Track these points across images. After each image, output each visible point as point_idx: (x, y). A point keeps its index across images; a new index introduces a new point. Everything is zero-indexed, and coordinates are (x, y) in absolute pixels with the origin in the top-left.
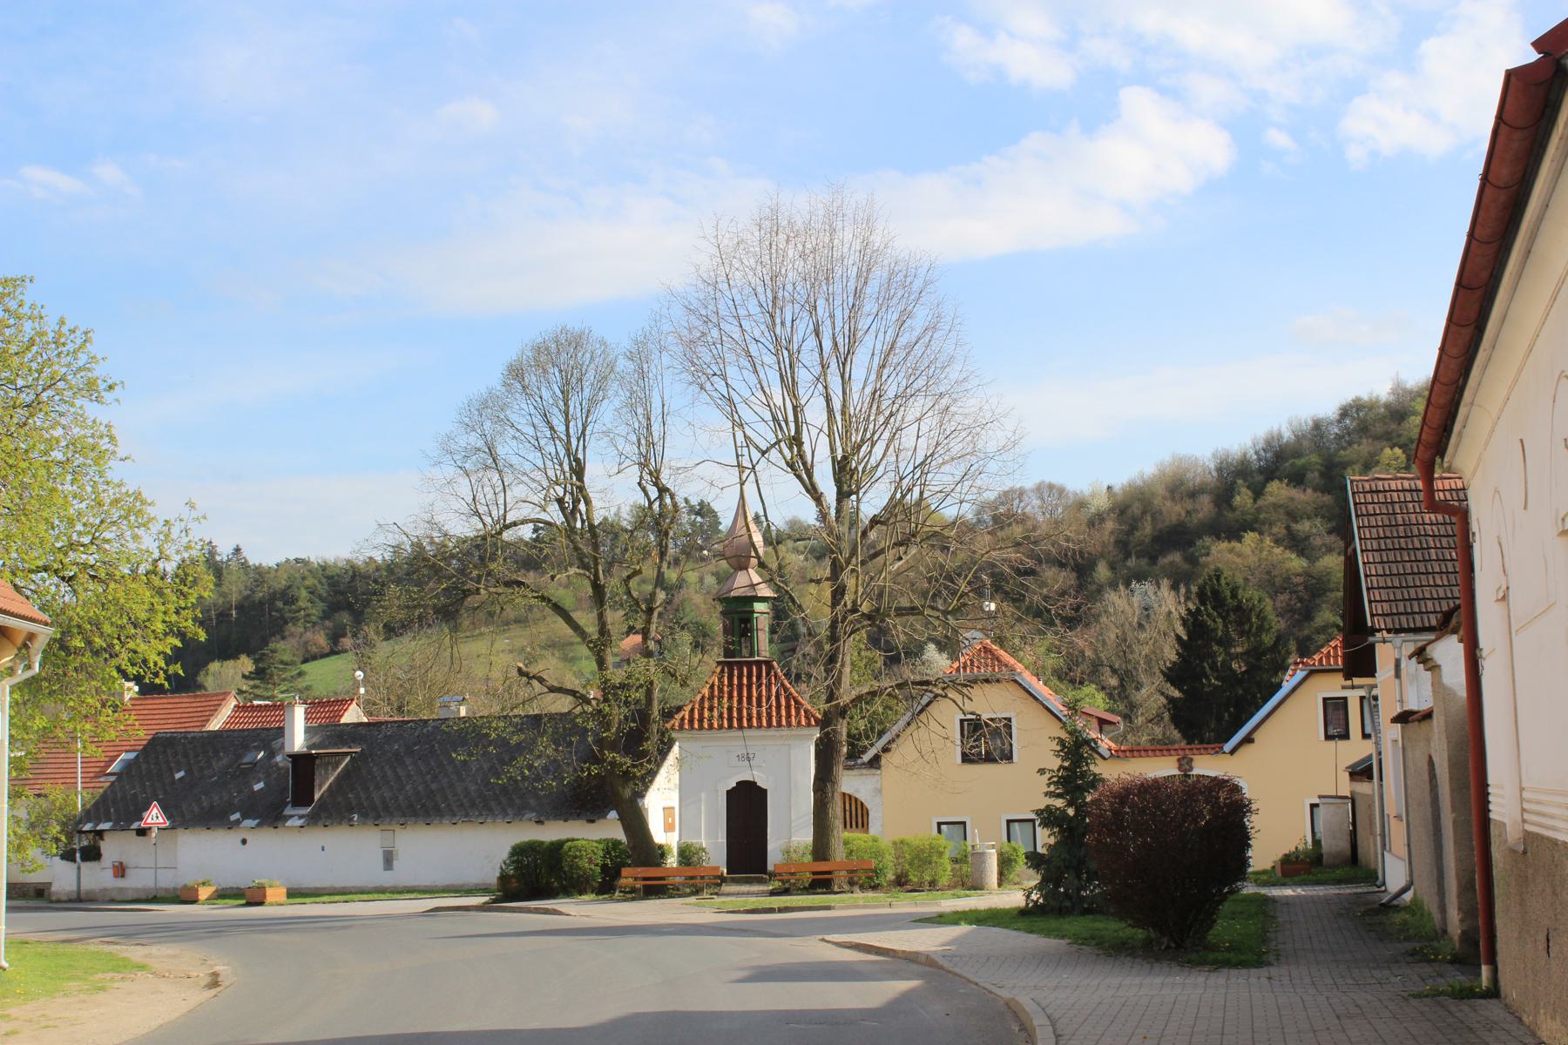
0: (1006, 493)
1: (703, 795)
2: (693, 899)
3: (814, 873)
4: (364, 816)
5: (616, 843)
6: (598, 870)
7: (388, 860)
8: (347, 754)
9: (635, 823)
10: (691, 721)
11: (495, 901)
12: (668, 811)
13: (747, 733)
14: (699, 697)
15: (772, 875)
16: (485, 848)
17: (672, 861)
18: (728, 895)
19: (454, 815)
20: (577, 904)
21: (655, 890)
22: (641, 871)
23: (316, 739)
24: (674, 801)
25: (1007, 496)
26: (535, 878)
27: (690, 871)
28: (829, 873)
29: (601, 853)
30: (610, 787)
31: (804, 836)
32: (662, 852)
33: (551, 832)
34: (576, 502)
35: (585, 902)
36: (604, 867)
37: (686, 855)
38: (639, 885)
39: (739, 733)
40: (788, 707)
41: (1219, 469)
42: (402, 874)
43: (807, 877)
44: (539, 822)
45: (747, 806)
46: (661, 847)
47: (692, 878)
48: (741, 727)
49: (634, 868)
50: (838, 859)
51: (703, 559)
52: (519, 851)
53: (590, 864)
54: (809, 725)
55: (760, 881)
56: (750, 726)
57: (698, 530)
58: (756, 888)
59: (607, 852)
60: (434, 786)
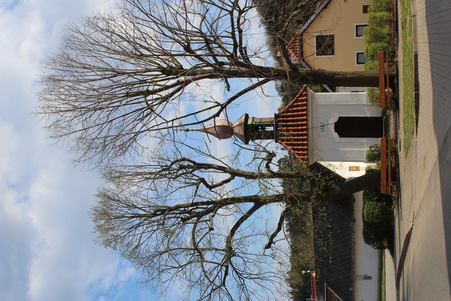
0: (276, 89)
1: (341, 149)
2: (401, 154)
3: (386, 86)
4: (350, 286)
5: (365, 195)
6: (379, 204)
7: (368, 278)
8: (327, 288)
9: (356, 183)
10: (303, 155)
11: (393, 253)
12: (351, 169)
13: (310, 126)
14: (292, 151)
15: (384, 113)
16: (365, 255)
17: (373, 165)
18: (396, 134)
19: (351, 253)
20: (400, 219)
21: (394, 175)
22: (383, 182)
23: (322, 298)
24: (347, 165)
25: (277, 89)
26: (382, 233)
27: (383, 155)
28: (385, 76)
29: (371, 202)
30: (339, 193)
31: (363, 95)
32: (369, 171)
33: (359, 226)
34: (184, 212)
35: (399, 214)
36: (378, 201)
37: (371, 158)
38: (390, 184)
39: (310, 130)
40: (298, 106)
41: (269, 35)
42: (373, 272)
43: (388, 90)
44: (354, 221)
45: (349, 127)
46: (367, 171)
47: (387, 155)
48: (307, 130)
49: (383, 186)
50: (378, 72)
51: (291, 162)
52: (368, 240)
53: (376, 208)
54: (306, 95)
55: (387, 119)
56: (306, 125)
57: (284, 163)
58: (392, 121)
59: (370, 199)
60: (339, 259)
